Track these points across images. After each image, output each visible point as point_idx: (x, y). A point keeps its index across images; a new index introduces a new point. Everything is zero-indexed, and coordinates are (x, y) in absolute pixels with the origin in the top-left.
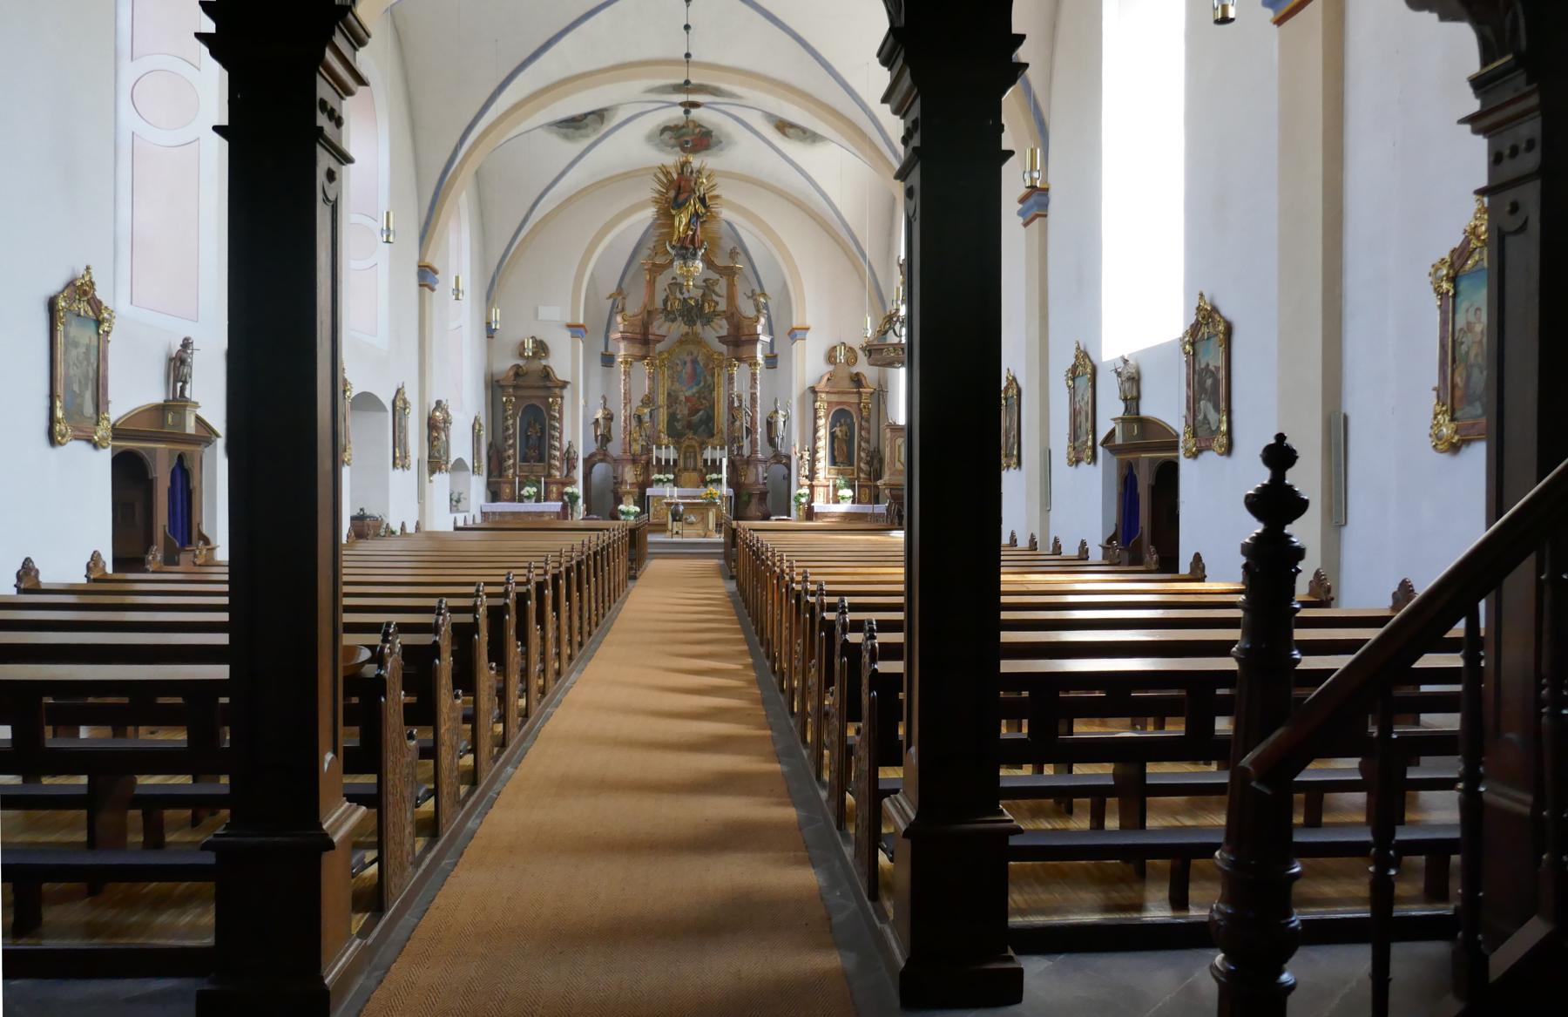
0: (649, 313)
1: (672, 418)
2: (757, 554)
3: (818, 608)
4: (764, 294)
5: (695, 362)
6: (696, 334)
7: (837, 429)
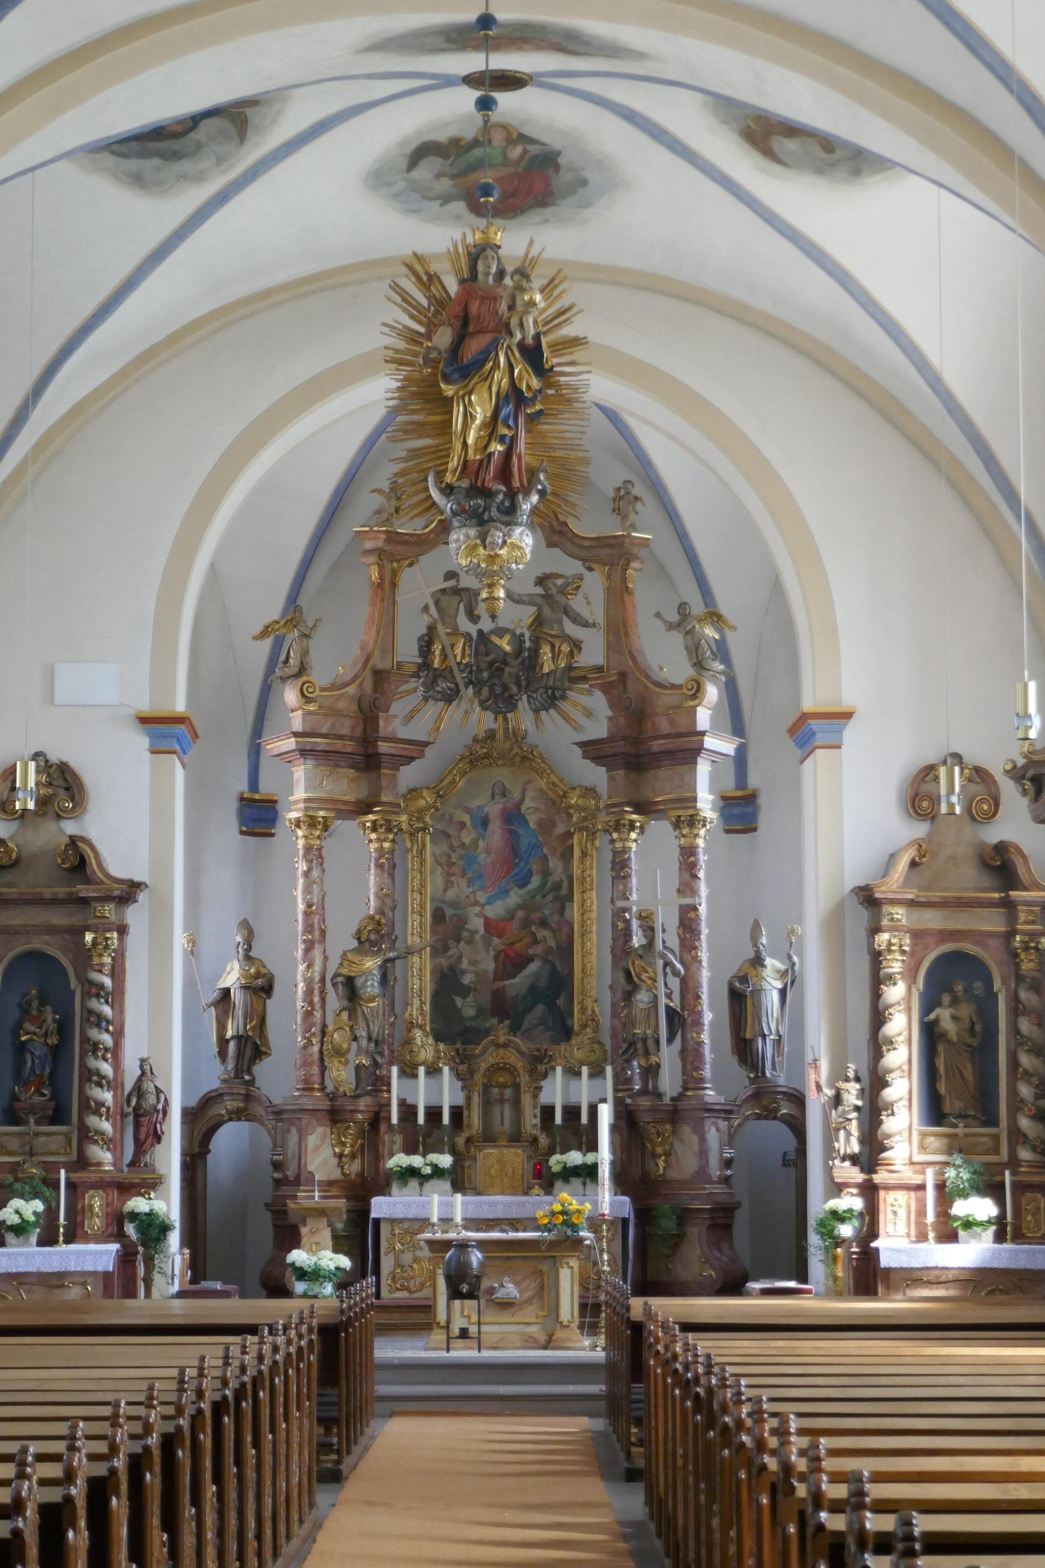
0: (379, 676)
1: (447, 984)
2: (706, 1406)
3: (852, 1547)
4: (715, 617)
5: (513, 817)
6: (517, 737)
7: (944, 1015)
